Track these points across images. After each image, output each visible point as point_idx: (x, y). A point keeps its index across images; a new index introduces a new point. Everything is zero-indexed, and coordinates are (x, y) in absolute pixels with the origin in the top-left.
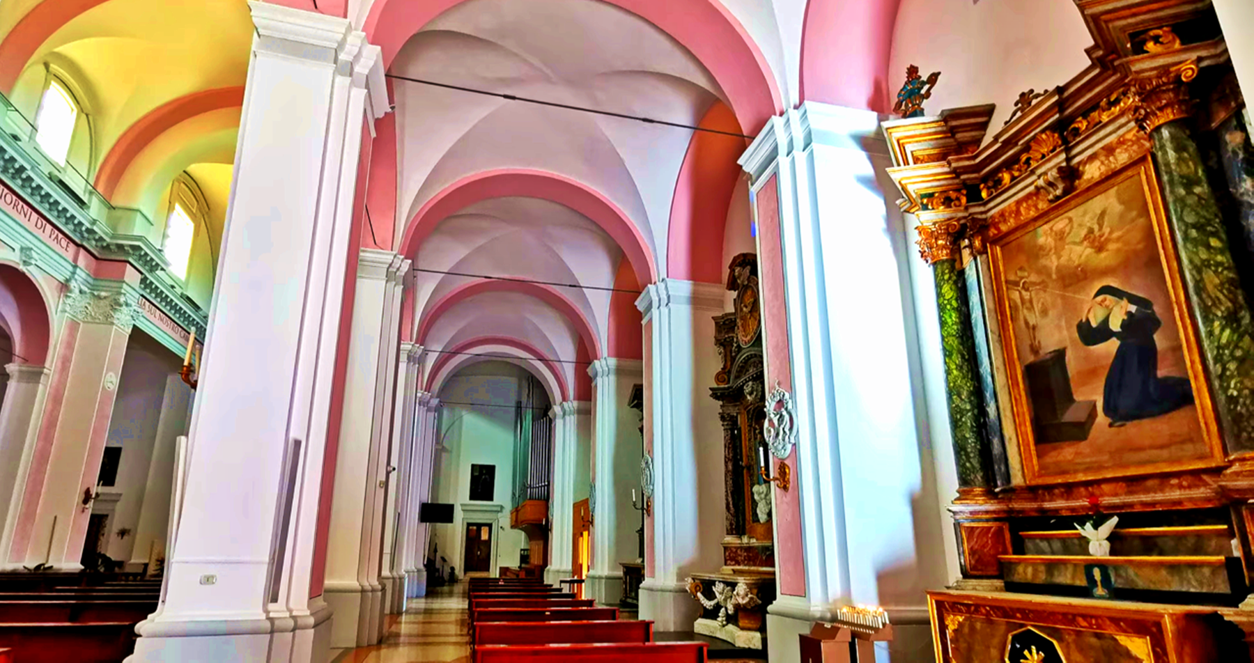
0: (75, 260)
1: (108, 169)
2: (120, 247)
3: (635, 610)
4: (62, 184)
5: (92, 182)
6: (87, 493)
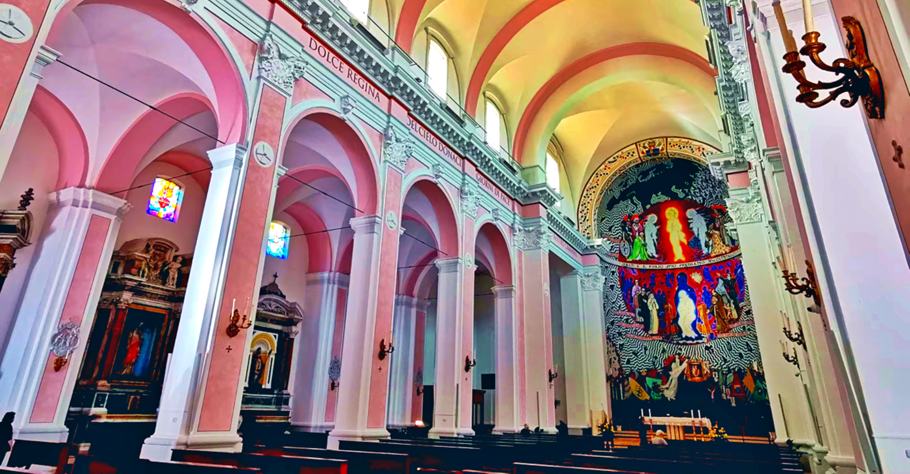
0: (513, 209)
1: (517, 145)
2: (534, 194)
3: (155, 415)
4: (448, 110)
5: (511, 154)
6: (467, 361)
